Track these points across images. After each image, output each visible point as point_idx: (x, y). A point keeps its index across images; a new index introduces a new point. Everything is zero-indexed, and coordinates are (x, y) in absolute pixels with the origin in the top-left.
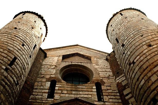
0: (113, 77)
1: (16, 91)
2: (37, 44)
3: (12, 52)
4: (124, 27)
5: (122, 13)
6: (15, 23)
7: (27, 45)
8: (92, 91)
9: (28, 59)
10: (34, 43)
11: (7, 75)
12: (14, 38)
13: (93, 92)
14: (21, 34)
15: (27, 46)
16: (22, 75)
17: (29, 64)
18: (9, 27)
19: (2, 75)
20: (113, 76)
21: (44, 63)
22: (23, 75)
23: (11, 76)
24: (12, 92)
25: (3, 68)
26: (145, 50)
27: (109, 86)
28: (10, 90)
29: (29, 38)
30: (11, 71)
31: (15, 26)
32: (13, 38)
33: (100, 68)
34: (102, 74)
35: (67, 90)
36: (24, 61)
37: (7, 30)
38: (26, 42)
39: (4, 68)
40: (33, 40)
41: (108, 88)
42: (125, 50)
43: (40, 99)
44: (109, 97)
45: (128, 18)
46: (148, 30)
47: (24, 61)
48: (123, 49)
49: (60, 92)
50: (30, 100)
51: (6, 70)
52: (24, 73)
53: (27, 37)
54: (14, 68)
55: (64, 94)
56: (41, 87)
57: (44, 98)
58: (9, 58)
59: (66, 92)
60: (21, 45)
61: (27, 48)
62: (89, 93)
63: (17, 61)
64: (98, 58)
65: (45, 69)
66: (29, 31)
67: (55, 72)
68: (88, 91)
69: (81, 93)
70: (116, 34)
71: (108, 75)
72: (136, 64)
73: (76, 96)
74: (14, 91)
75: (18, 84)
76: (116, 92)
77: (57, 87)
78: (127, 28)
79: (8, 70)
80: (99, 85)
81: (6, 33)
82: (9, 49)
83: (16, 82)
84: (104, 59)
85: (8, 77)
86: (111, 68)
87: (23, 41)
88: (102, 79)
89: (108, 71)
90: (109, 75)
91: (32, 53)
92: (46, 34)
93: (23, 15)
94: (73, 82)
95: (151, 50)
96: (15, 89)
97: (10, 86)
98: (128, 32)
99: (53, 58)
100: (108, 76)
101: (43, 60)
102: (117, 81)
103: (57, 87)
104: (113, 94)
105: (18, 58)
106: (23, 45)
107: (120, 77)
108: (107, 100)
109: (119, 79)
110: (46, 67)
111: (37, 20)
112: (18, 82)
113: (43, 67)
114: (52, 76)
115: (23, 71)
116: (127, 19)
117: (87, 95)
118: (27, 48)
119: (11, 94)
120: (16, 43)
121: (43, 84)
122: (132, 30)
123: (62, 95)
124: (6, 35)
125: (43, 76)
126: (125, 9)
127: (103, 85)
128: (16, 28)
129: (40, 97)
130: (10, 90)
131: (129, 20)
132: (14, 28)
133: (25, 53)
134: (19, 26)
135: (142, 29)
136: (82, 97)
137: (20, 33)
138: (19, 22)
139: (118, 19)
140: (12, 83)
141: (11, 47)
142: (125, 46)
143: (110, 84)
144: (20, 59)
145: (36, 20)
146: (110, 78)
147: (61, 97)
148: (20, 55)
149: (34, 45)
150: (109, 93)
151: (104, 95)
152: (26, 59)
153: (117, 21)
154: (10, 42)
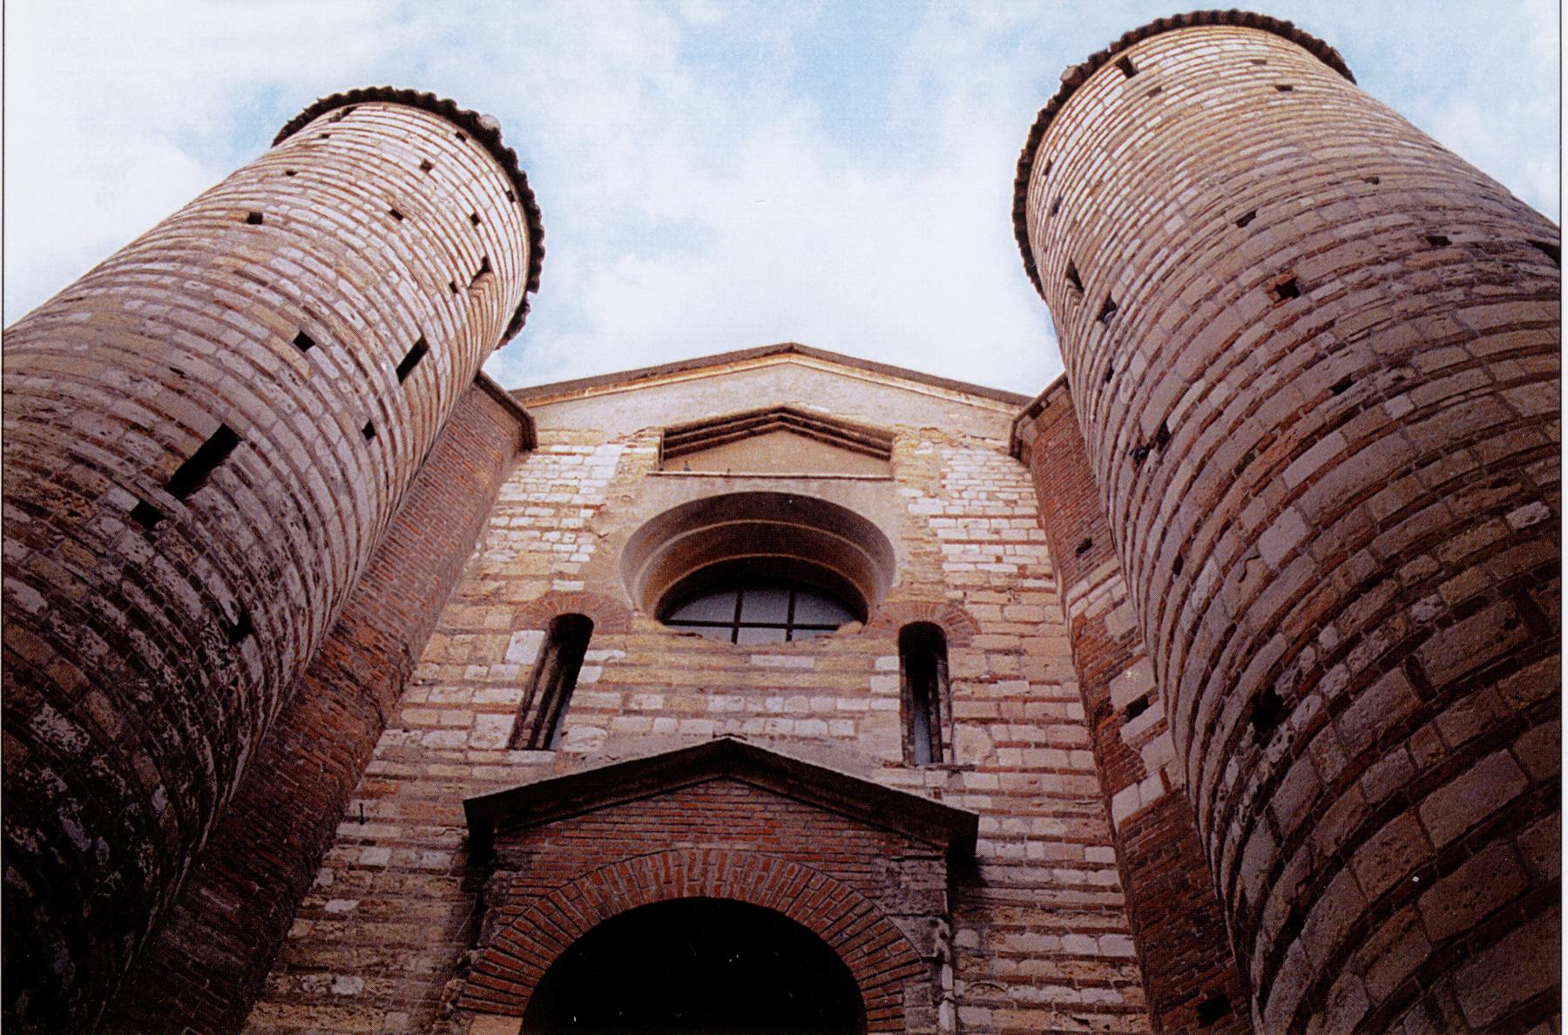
0: (1051, 585)
1: (235, 683)
2: (429, 340)
3: (201, 393)
4: (1129, 165)
5: (1135, 61)
6: (260, 181)
7: (343, 343)
8: (865, 692)
9: (343, 449)
10: (401, 332)
11: (150, 560)
12: (227, 288)
13: (877, 695)
14: (294, 261)
15: (337, 351)
16: (292, 568)
17: (358, 487)
18: (207, 214)
19: (104, 555)
20: (1050, 577)
21: (508, 492)
22: (299, 568)
23: (182, 569)
24: (193, 689)
25: (115, 508)
26: (1248, 326)
27: (1007, 652)
28: (167, 670)
29: (358, 289)
30: (181, 528)
31: (255, 206)
32: (220, 293)
33: (957, 517)
34: (960, 563)
35: (669, 685)
36: (303, 461)
37: (189, 232)
38: (335, 322)
39: (129, 503)
40: (400, 308)
41: (1004, 664)
42: (1118, 343)
43: (457, 755)
44: (999, 732)
45: (1170, 92)
46: (1304, 166)
47: (303, 461)
48: (1104, 343)
49: (613, 698)
50: (375, 767)
51: (145, 517)
52: (307, 554)
53: (343, 285)
54: (214, 509)
55: (639, 713)
56: (472, 670)
57: (485, 744)
58: (169, 431)
59: (656, 702)
60: (285, 339)
61: (338, 365)
62: (842, 704)
63: (242, 458)
64: (951, 443)
65: (515, 535)
66: (365, 233)
67: (586, 559)
68: (834, 692)
69: (774, 704)
70: (1070, 230)
71: (1015, 570)
72: (1176, 446)
73: (732, 727)
74: (214, 683)
75: (247, 626)
76: (1056, 691)
77: (594, 664)
78: (1149, 168)
79: (162, 518)
80: (923, 650)
81: (173, 253)
82: (181, 373)
83: (230, 612)
84: (998, 444)
85: (155, 569)
86: (1046, 515)
87: (301, 315)
88: (962, 602)
89: (1022, 536)
90: (1022, 567)
91: (381, 402)
92: (534, 269)
93: (331, 121)
94: (741, 630)
95: (1295, 318)
96: (222, 667)
97: (169, 636)
98: (1151, 199)
99: (590, 449)
100: (1010, 576)
101: (499, 478)
102: (1074, 612)
103: (594, 664)
104: (1033, 709)
105: (254, 435)
106: (304, 342)
107: (1097, 576)
108: (979, 756)
109: (1092, 589)
110: (524, 522)
111: (445, 157)
112: (244, 613)
113: (502, 521)
114: (563, 589)
115: (299, 536)
116: (1162, 96)
117: (824, 717)
118: (338, 365)
119: (183, 699)
120: (245, 324)
121: (490, 645)
122: (1187, 182)
123: (623, 723)
124: (164, 273)
125: (492, 585)
126: (1160, 27)
127: (961, 645)
128: (255, 218)
129: (454, 739)
130: (167, 670)
131: (1174, 110)
132: (245, 216)
133: (321, 398)
134: (281, 198)
135: (1262, 164)
136: (783, 737)
137: (283, 250)
138: (291, 173)
139: (1100, 108)
140: (195, 616)
141: (199, 355)
142: (1120, 312)
143: (1022, 636)
144: (265, 445)
145: (436, 151)
146: (1030, 590)
147: (614, 737)
148: (268, 417)
149: (409, 347)
150: (1003, 705)
151: (963, 721)
152: (329, 444)
153: (1086, 124)
154: (196, 321)
